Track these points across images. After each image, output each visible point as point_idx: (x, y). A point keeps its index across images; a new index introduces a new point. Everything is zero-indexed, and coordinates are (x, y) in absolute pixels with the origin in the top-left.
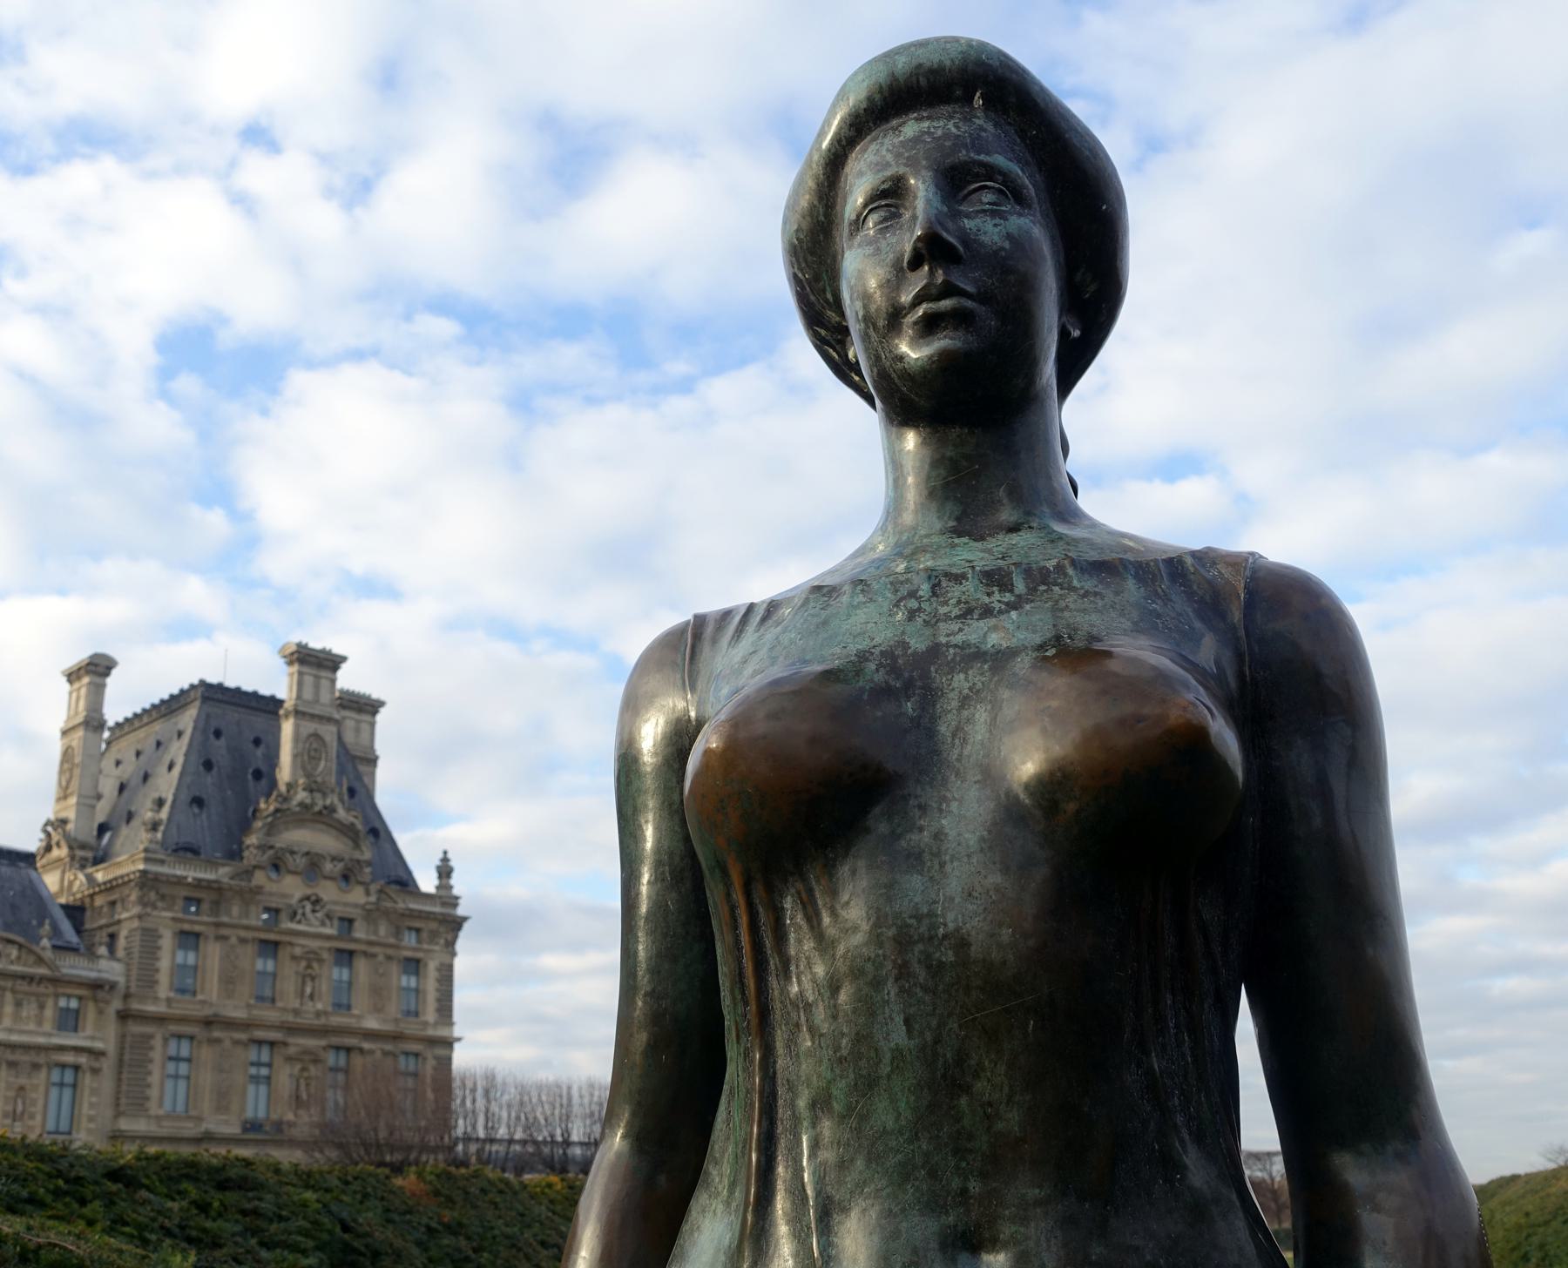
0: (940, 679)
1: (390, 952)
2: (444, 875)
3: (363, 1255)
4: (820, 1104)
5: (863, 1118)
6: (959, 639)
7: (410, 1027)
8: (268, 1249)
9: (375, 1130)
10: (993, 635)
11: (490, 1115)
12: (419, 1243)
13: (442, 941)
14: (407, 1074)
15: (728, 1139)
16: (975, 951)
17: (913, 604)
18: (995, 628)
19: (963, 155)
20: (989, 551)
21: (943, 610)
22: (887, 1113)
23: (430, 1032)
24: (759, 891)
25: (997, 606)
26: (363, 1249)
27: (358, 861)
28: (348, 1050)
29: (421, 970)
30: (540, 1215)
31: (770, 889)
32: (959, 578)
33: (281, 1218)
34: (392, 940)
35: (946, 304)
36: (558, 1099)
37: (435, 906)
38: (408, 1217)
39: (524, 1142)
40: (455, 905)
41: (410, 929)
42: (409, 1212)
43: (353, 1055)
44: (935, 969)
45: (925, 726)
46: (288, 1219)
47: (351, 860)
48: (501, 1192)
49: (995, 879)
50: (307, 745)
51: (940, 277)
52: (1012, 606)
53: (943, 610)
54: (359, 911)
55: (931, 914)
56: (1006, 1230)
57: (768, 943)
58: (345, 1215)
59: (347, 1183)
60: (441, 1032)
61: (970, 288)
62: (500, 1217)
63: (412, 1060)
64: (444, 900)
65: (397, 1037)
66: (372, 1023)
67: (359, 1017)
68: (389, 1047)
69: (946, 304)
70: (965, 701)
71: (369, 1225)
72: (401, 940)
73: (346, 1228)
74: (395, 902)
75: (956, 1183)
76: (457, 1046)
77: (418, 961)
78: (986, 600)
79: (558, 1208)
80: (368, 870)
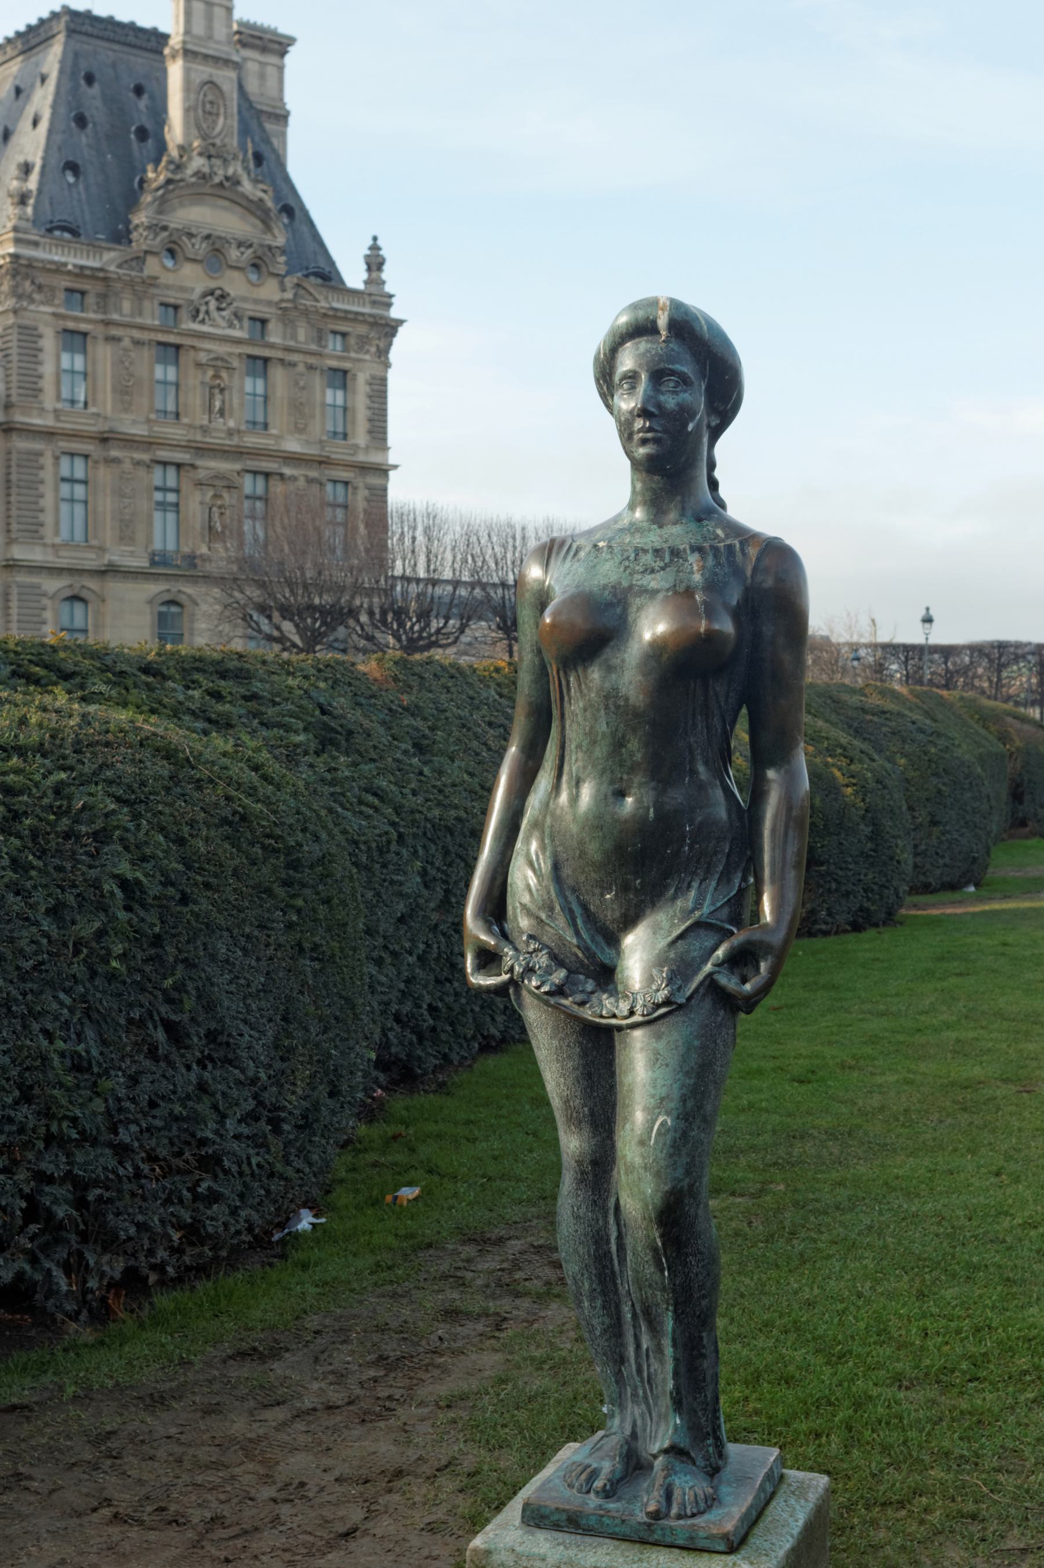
0: (631, 600)
4: (579, 746)
10: (653, 582)
15: (853, 777)
16: (631, 702)
17: (627, 563)
19: (662, 365)
22: (600, 751)
24: (562, 674)
35: (649, 435)
44: (618, 707)
49: (640, 678)
52: (663, 569)
56: (633, 791)
69: (649, 435)
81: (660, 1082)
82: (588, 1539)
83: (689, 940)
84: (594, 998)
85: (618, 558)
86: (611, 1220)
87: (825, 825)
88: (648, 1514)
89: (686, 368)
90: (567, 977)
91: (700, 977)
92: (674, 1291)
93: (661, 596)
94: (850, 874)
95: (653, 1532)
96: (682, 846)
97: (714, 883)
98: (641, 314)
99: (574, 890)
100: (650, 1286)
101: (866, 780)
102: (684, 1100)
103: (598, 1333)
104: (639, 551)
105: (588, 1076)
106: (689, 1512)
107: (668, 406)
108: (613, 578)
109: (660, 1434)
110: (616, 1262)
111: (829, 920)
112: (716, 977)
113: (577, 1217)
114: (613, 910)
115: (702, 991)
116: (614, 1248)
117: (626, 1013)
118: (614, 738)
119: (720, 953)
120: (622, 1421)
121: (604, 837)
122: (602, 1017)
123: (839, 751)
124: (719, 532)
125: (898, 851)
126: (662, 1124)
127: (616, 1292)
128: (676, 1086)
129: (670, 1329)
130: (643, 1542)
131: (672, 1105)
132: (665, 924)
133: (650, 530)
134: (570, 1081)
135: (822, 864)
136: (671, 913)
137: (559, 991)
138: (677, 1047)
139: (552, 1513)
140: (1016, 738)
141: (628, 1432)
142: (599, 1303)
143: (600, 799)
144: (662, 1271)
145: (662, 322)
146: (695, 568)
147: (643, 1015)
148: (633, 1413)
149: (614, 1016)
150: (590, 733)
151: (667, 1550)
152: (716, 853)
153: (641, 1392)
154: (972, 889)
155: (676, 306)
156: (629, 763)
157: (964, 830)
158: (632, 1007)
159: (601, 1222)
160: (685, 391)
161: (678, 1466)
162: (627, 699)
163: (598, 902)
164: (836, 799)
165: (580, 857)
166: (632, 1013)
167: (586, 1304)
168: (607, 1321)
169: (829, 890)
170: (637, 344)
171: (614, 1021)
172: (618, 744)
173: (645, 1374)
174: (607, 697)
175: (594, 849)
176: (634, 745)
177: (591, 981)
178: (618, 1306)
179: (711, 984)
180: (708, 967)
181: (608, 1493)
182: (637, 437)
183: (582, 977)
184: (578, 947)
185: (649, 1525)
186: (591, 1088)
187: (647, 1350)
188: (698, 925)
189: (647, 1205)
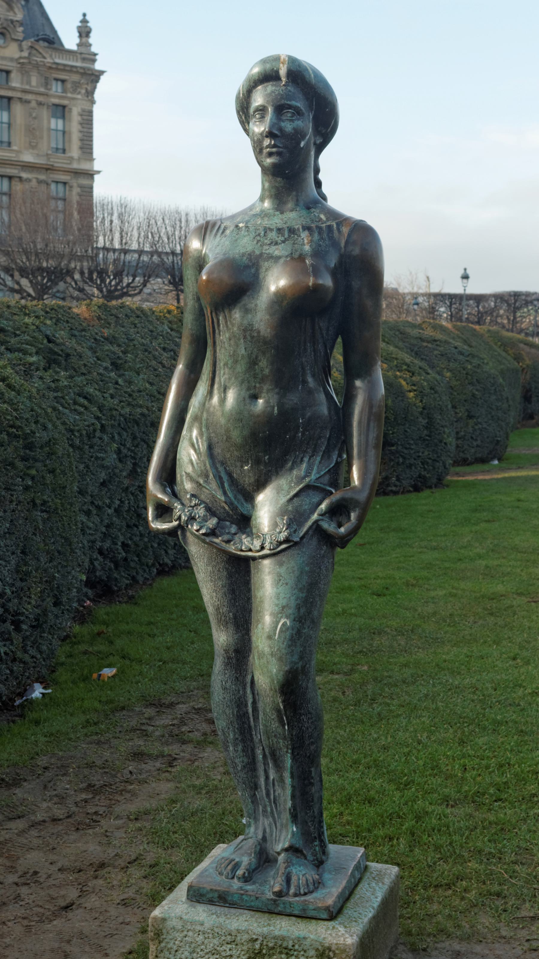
0: (261, 263)
1: (41, 99)
2: (84, 35)
3: (59, 355)
4: (226, 364)
5: (234, 369)
6: (267, 252)
7: (59, 161)
8: (11, 352)
9: (34, 242)
10: (276, 251)
11: (123, 234)
12: (91, 348)
13: (83, 91)
14: (57, 199)
15: (414, 385)
16: (262, 334)
17: (258, 238)
18: (277, 249)
19: (283, 102)
20: (282, 219)
21: (266, 241)
22: (240, 368)
23: (75, 166)
24: (214, 314)
25: (279, 241)
26: (60, 353)
27: (12, 21)
28: (10, 178)
29: (67, 114)
30: (162, 331)
31: (217, 314)
32: (271, 230)
33: (16, 335)
34: (42, 90)
35: (274, 150)
36: (178, 223)
37: (77, 61)
38: (83, 333)
39: (152, 254)
40: (94, 61)
41: (57, 80)
42: (84, 330)
43: (13, 183)
44: (253, 337)
46: (19, 335)
47: (6, 20)
48: (138, 317)
49: (268, 317)
50: (301, 769)
52: (284, 242)
53: (266, 241)
54: (14, 64)
55: (252, 325)
58: (48, 333)
59: (47, 312)
60: (84, 166)
61: (281, 145)
62: (138, 333)
63: (61, 187)
64: (83, 56)
65: (49, 169)
66: (28, 157)
67: (18, 152)
68: (42, 177)
69: (274, 150)
71: (62, 339)
72: (50, 89)
73: (49, 341)
74: (44, 58)
75: (253, 384)
76: (96, 177)
77: (64, 107)
78: (277, 239)
79: (175, 326)
80: (21, 29)
81: (282, 595)
82: (233, 911)
83: (302, 498)
84: (236, 538)
85: (253, 235)
86: (249, 690)
87: (395, 419)
89: (299, 103)
91: (309, 523)
92: (292, 739)
94: (412, 452)
95: (278, 905)
96: (297, 433)
97: (319, 459)
98: (268, 66)
100: (275, 736)
101: (423, 387)
102: (298, 607)
103: (239, 769)
104: (267, 230)
105: (232, 591)
106: (302, 892)
107: (287, 130)
108: (249, 248)
110: (252, 720)
111: (398, 483)
112: (321, 523)
113: (225, 689)
115: (310, 533)
116: (250, 710)
117: (258, 548)
119: (323, 506)
120: (256, 829)
122: (242, 550)
123: (405, 367)
124: (322, 216)
125: (445, 436)
126: (283, 625)
127: (252, 740)
130: (271, 912)
131: (290, 611)
132: (286, 487)
133: (274, 215)
134: (220, 595)
135: (393, 445)
136: (289, 479)
137: (212, 533)
138: (293, 571)
139: (208, 892)
140: (526, 358)
142: (240, 748)
143: (240, 401)
144: (283, 726)
145: (283, 72)
146: (306, 241)
147: (270, 549)
148: (263, 824)
149: (250, 550)
150: (234, 355)
151: (287, 918)
152: (320, 438)
154: (496, 462)
155: (292, 60)
156: (260, 376)
157: (490, 422)
159: (241, 692)
160: (298, 120)
162: (259, 332)
163: (239, 472)
164: (403, 400)
165: (227, 440)
166: (262, 548)
167: (231, 748)
168: (246, 760)
169: (398, 464)
170: (265, 87)
171: (250, 554)
172: (253, 363)
173: (272, 797)
174: (245, 331)
175: (236, 435)
176: (264, 363)
177: (234, 526)
178: (253, 750)
179: (317, 528)
180: (315, 517)
182: (266, 151)
183: (228, 523)
184: (226, 503)
185: (275, 901)
186: (235, 599)
188: (308, 487)
189: (273, 680)
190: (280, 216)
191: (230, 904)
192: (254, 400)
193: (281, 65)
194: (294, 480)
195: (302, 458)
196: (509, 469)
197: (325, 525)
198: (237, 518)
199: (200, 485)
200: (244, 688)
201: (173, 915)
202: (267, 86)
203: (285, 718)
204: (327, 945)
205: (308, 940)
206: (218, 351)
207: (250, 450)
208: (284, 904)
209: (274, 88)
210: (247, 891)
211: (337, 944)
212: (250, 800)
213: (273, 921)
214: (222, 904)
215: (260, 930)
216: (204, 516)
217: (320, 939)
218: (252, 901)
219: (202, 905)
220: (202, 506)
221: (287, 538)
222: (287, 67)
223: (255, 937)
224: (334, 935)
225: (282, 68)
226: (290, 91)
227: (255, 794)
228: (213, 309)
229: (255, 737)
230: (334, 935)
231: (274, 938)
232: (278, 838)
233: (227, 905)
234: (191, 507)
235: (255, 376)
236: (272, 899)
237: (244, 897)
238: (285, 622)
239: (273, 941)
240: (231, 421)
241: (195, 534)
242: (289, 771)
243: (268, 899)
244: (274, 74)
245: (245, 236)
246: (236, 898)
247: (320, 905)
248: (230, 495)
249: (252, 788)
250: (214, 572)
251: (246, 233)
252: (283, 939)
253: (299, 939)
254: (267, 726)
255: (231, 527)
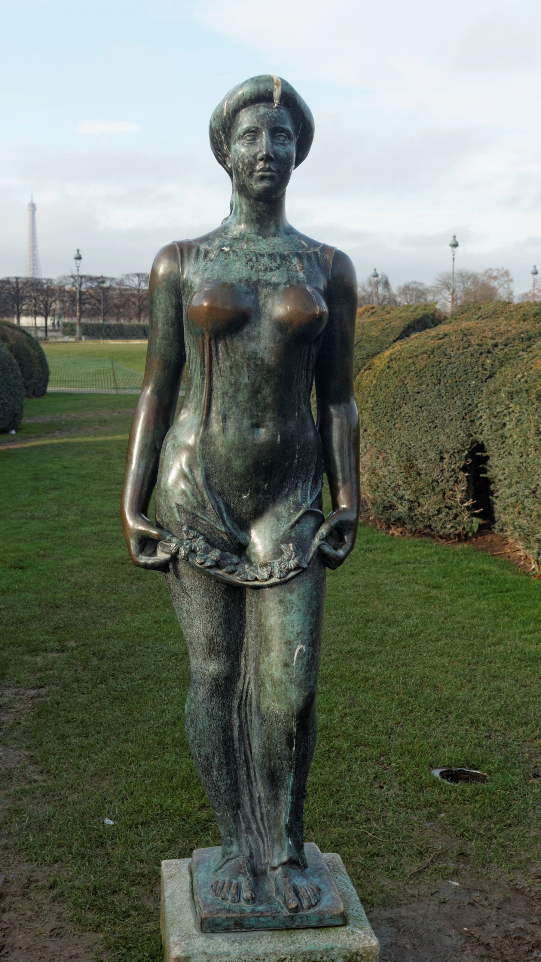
0: (260, 290)
4: (225, 393)
6: (264, 278)
10: (275, 277)
16: (266, 362)
17: (251, 264)
18: (273, 275)
19: (277, 125)
20: (268, 245)
22: (241, 397)
24: (213, 342)
25: (274, 268)
35: (268, 174)
44: (256, 366)
45: (256, 301)
49: (272, 345)
51: (267, 166)
52: (278, 268)
53: (260, 267)
55: (256, 353)
57: (214, 354)
69: (268, 174)
70: (266, 297)
75: (256, 413)
78: (270, 265)
81: (296, 623)
82: (250, 934)
84: (239, 568)
85: (244, 260)
86: (235, 715)
88: (290, 910)
89: (289, 127)
90: (221, 555)
92: (297, 759)
93: (281, 287)
95: (295, 921)
96: (294, 460)
97: (310, 483)
98: (262, 87)
99: (220, 494)
103: (222, 791)
106: (314, 903)
107: (280, 153)
109: (275, 853)
110: (237, 743)
113: (211, 716)
114: (248, 506)
115: (314, 558)
117: (266, 575)
118: (253, 387)
119: (323, 530)
120: (240, 846)
121: (247, 456)
122: (247, 580)
126: (300, 651)
127: (235, 762)
128: (307, 623)
129: (291, 784)
130: (288, 929)
131: (305, 637)
132: (285, 514)
133: (259, 241)
134: (215, 625)
137: (217, 565)
138: (304, 597)
139: (223, 921)
140: (11, 339)
141: (247, 854)
142: (224, 771)
144: (291, 748)
145: (277, 94)
146: (298, 268)
147: (280, 578)
148: (247, 841)
149: (256, 579)
150: (235, 383)
152: (310, 464)
153: (254, 827)
154: (13, 432)
155: (285, 84)
156: (262, 404)
157: (10, 397)
158: (271, 573)
159: (227, 717)
161: (293, 872)
162: (263, 360)
163: (236, 501)
166: (271, 576)
168: (229, 782)
170: (257, 108)
171: (257, 583)
172: (256, 391)
175: (238, 465)
176: (266, 391)
177: (234, 556)
179: (320, 552)
180: (316, 541)
181: (252, 900)
182: (256, 174)
183: (228, 553)
184: (226, 533)
185: (292, 917)
186: (229, 628)
187: (259, 797)
188: (308, 513)
189: (292, 707)
190: (264, 241)
191: (246, 928)
192: (256, 429)
193: (276, 87)
194: (292, 506)
195: (296, 484)
196: (30, 438)
197: (327, 549)
198: (234, 548)
199: (197, 516)
200: (230, 713)
201: (196, 951)
202: (259, 107)
203: (294, 740)
204: (354, 951)
205: (336, 949)
206: (214, 379)
207: (251, 479)
208: (301, 918)
209: (266, 110)
210: (262, 913)
211: (363, 948)
212: (232, 820)
213: (295, 937)
214: (239, 930)
215: (287, 949)
216: (205, 548)
217: (347, 946)
218: (269, 921)
219: (217, 934)
220: (200, 538)
221: (297, 565)
222: (282, 89)
223: (283, 957)
224: (357, 940)
225: (277, 90)
226: (282, 114)
227: (237, 813)
228: (213, 336)
229: (238, 759)
230: (357, 940)
231: (303, 954)
232: (266, 853)
233: (244, 930)
234: (189, 539)
235: (257, 405)
236: (289, 916)
237: (261, 919)
238: (302, 649)
239: (301, 957)
240: (234, 450)
241: (197, 567)
242: (290, 788)
243: (285, 917)
244: (267, 95)
245: (235, 261)
246: (252, 921)
247: (335, 913)
248: (229, 525)
249: (234, 808)
250: (210, 603)
251: (236, 258)
252: (311, 953)
253: (327, 951)
254: (270, 749)
255: (232, 557)
